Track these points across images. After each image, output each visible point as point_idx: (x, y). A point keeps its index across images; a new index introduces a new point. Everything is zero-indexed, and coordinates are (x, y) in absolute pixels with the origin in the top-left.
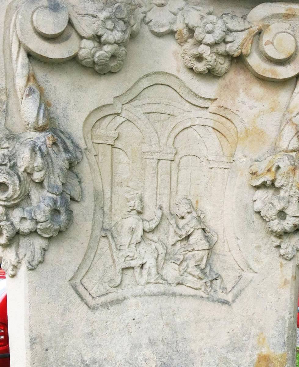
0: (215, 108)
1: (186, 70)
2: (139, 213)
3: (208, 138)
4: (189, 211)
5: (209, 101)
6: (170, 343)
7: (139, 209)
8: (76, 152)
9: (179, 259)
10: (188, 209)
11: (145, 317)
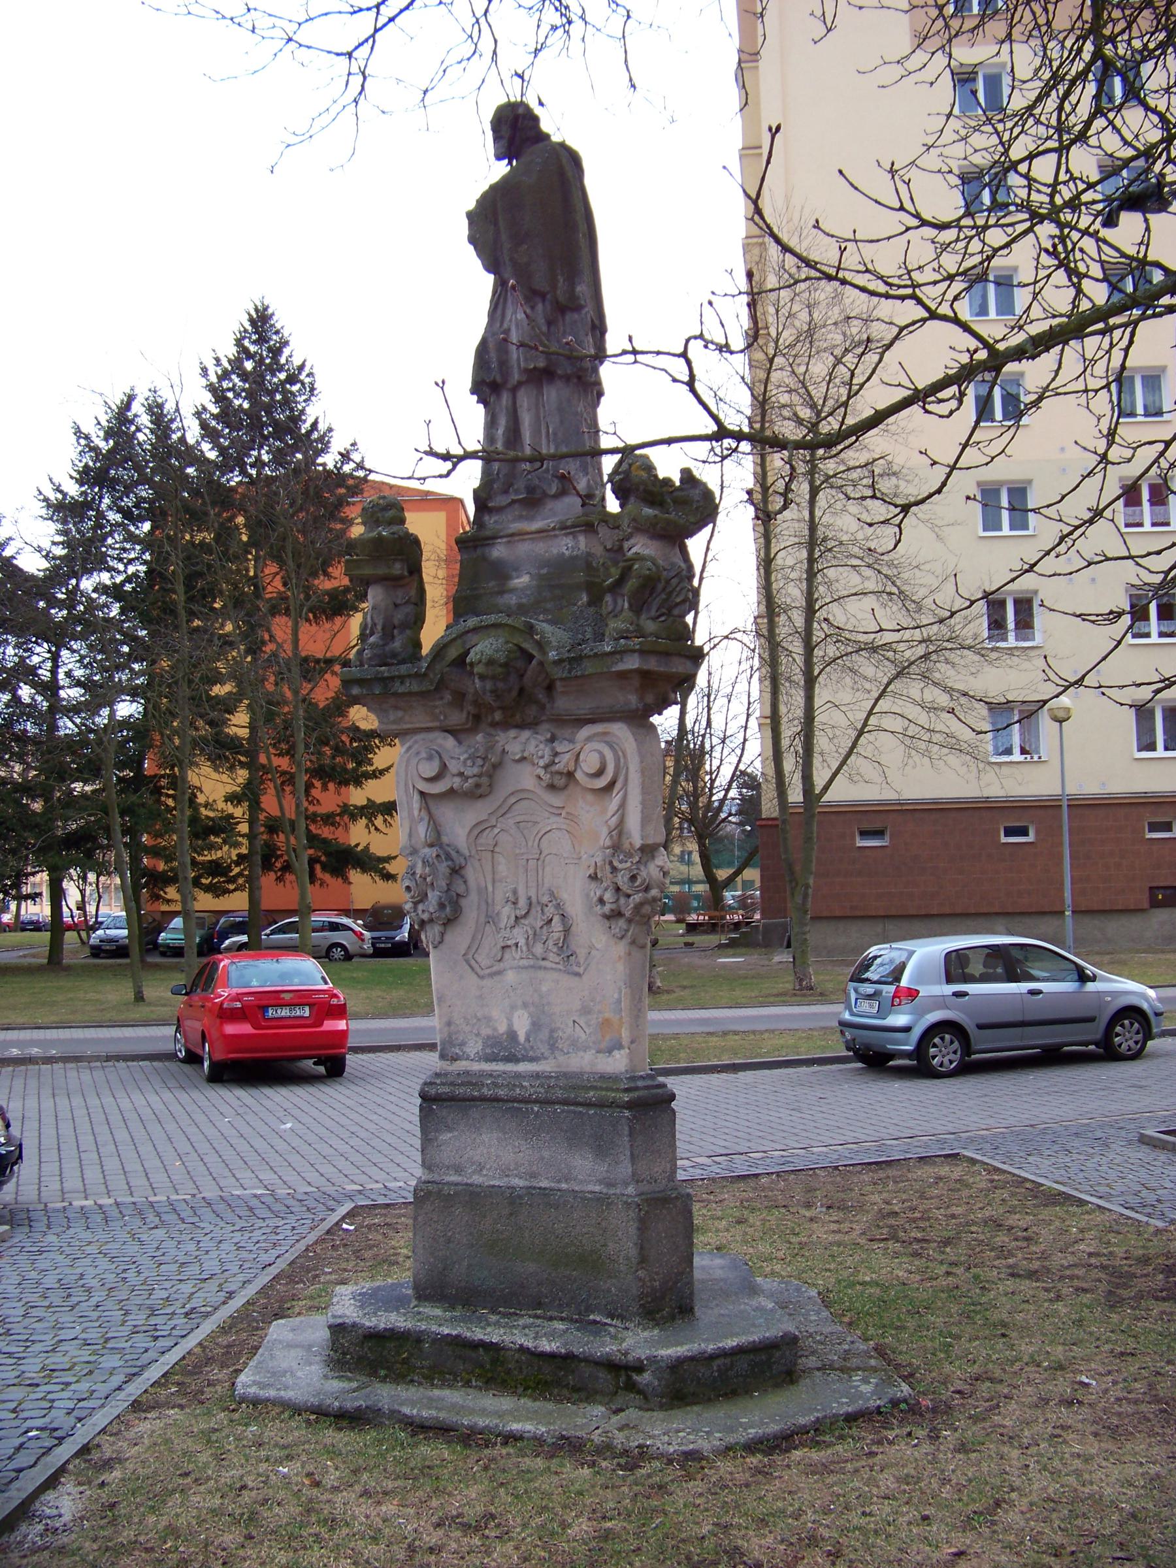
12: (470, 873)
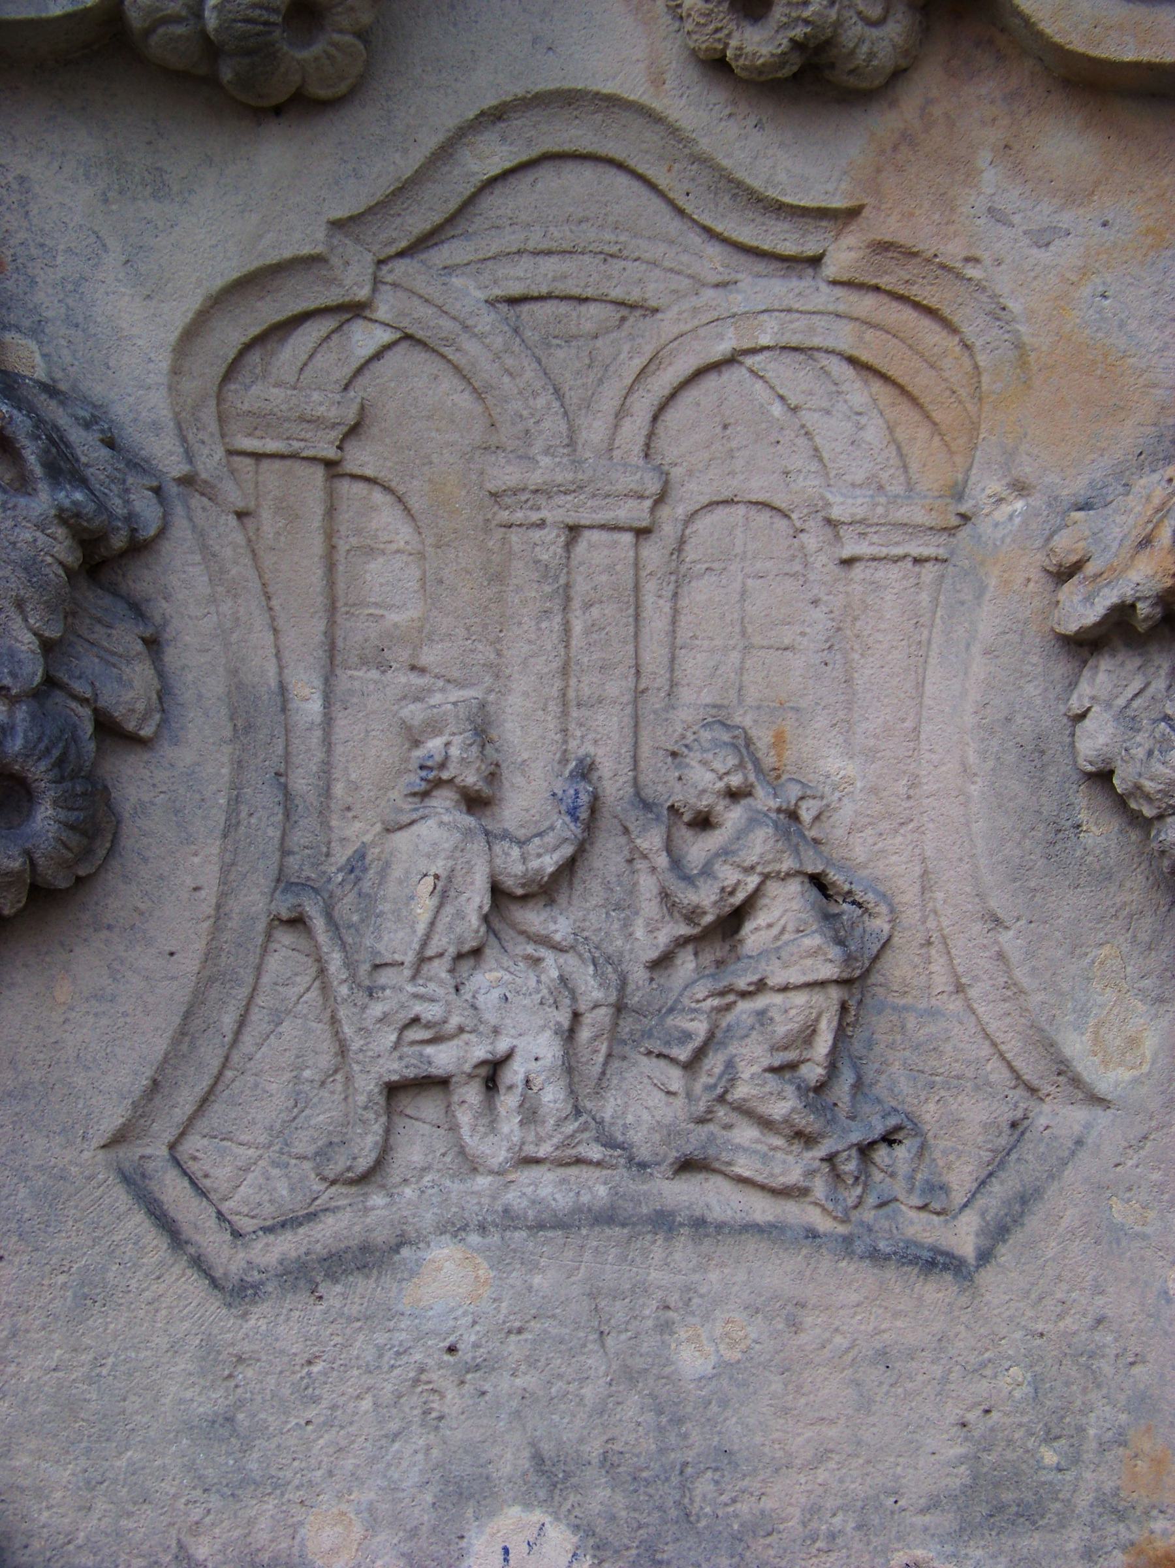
0: (853, 255)
1: (692, 74)
2: (475, 802)
3: (828, 412)
4: (735, 781)
5: (824, 224)
6: (645, 1474)
7: (471, 779)
8: (127, 491)
9: (687, 1036)
10: (727, 773)
11: (513, 1338)
12: (188, 585)
